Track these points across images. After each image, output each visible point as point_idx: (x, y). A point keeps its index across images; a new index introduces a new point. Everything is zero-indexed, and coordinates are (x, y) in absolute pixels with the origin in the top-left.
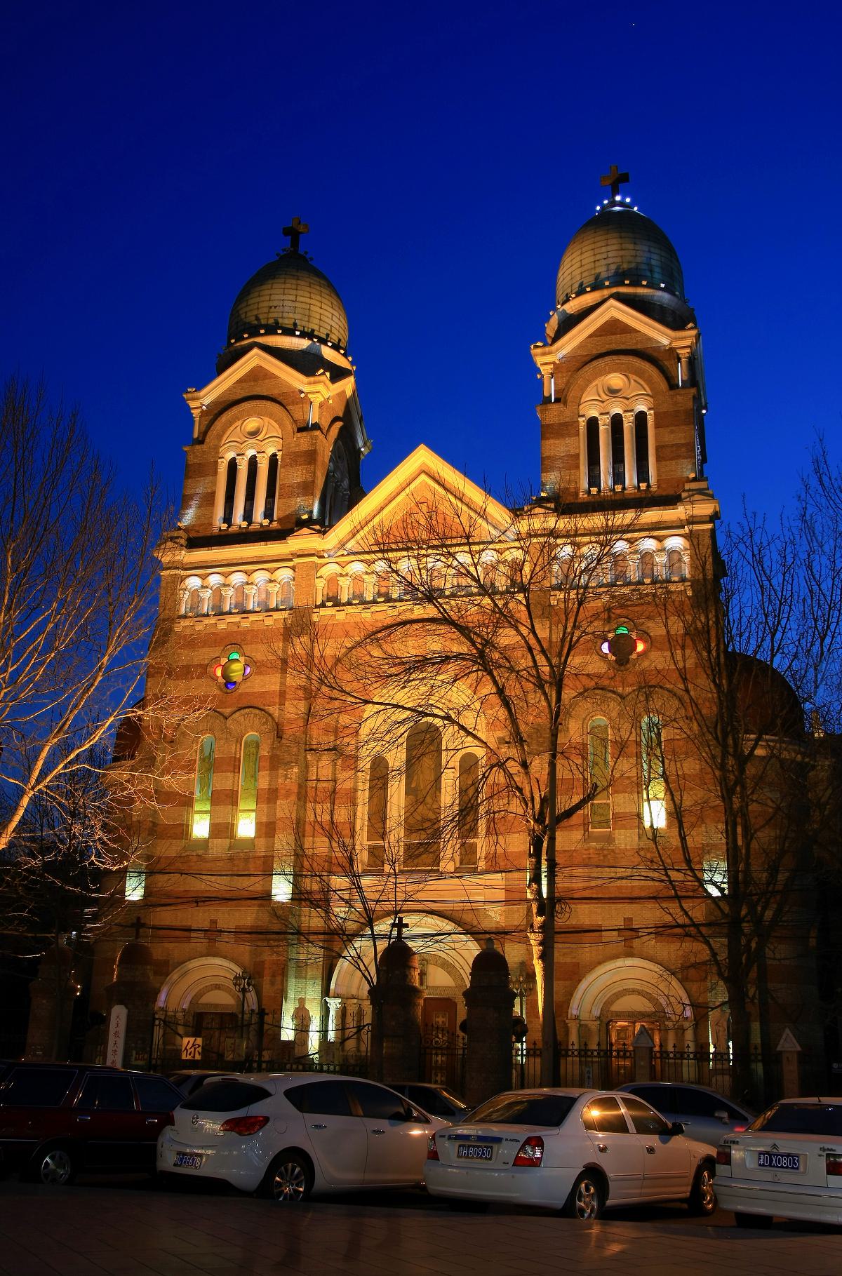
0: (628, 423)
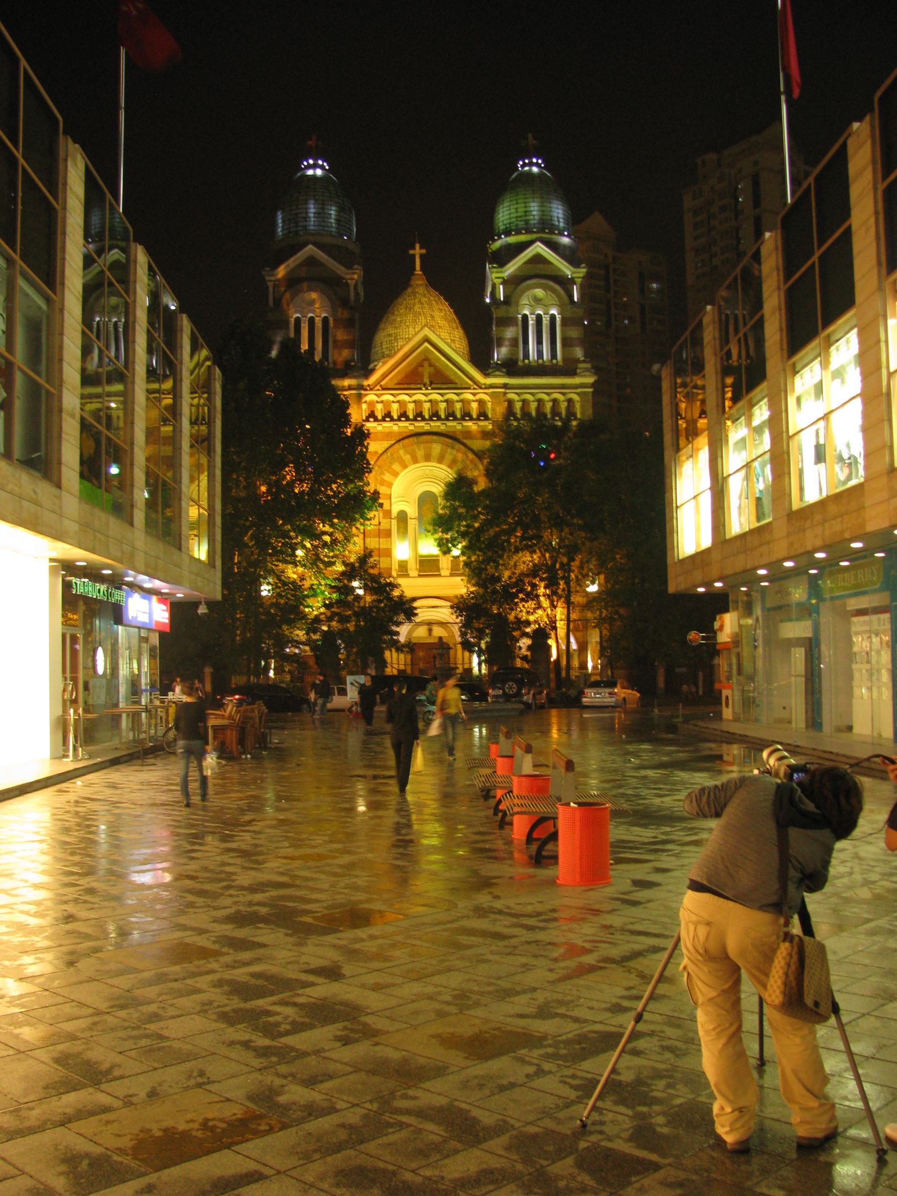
0: (546, 321)
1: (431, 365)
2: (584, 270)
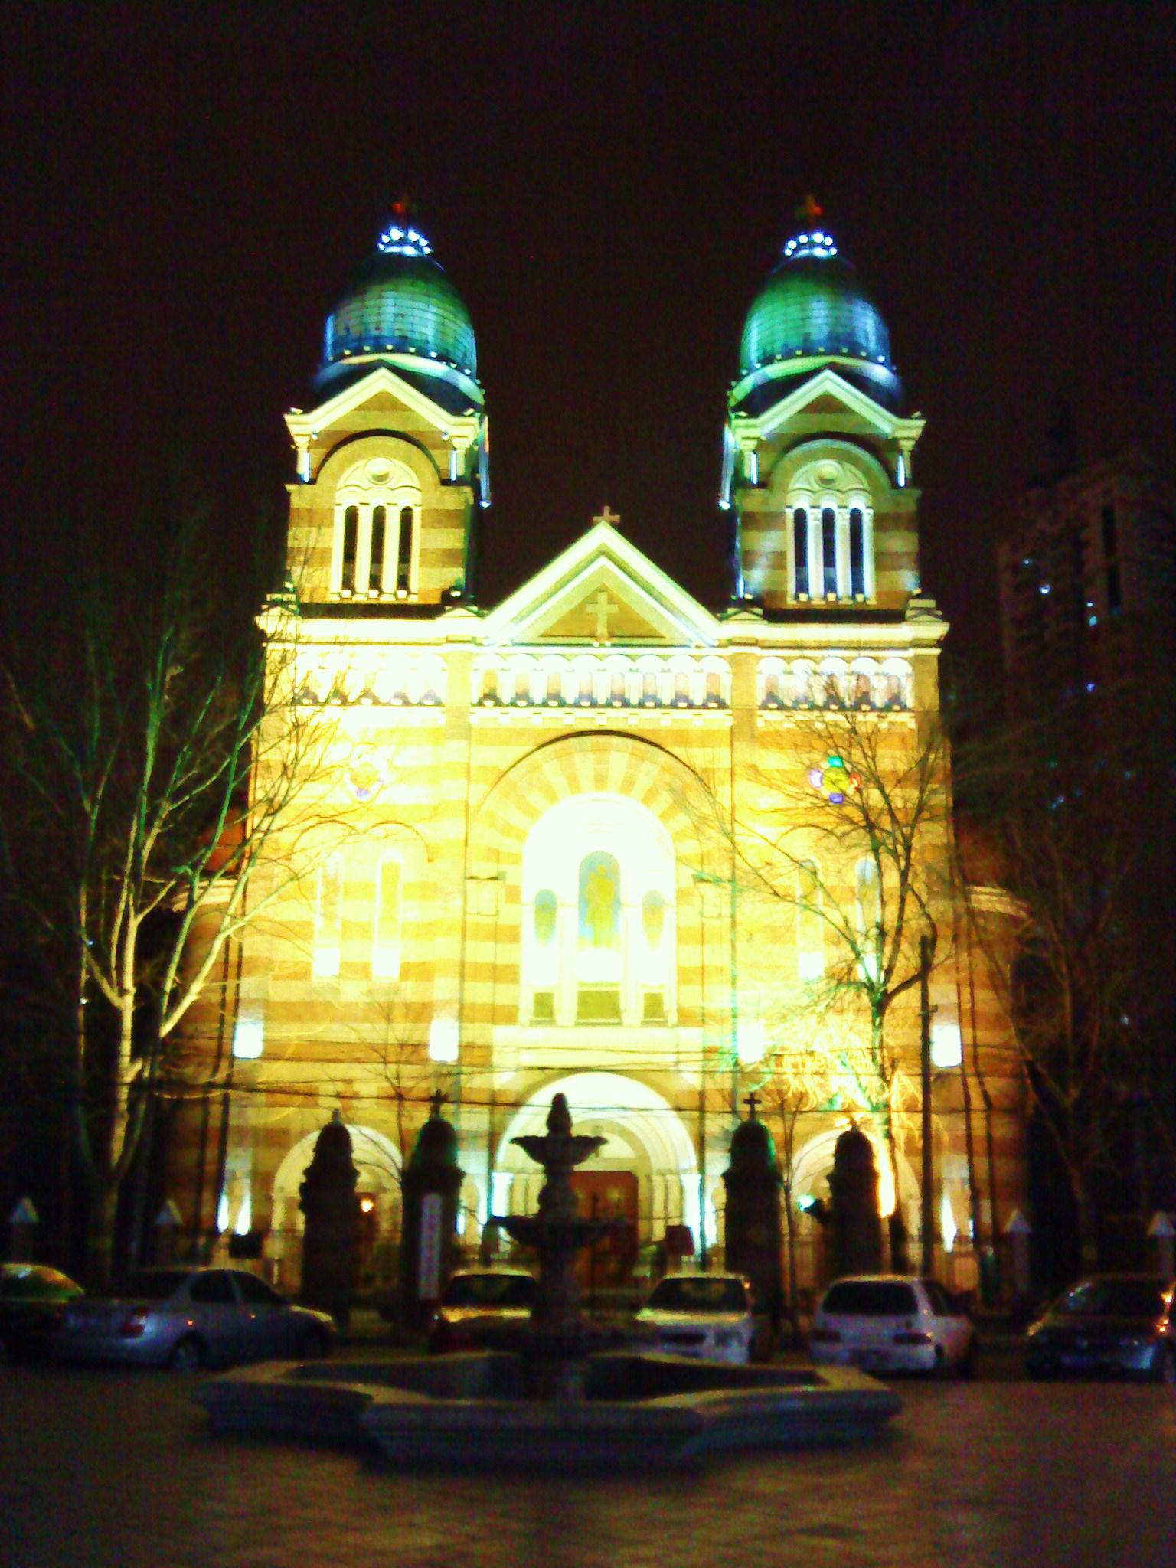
1: (611, 601)
2: (922, 423)
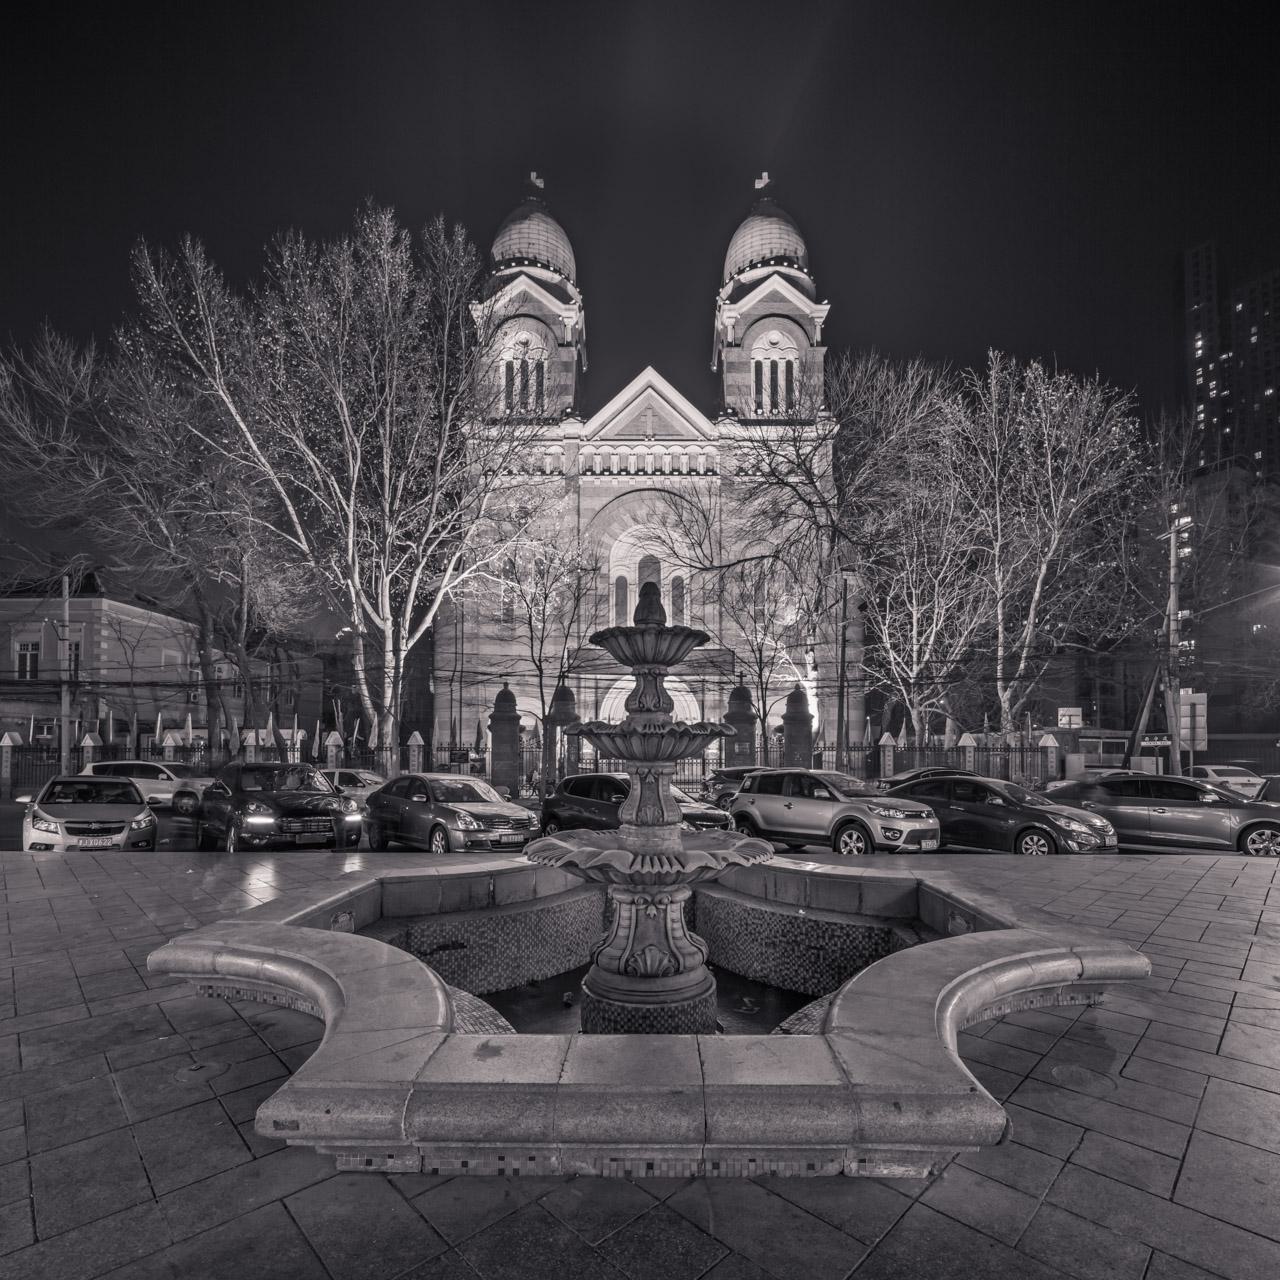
0: (782, 367)
